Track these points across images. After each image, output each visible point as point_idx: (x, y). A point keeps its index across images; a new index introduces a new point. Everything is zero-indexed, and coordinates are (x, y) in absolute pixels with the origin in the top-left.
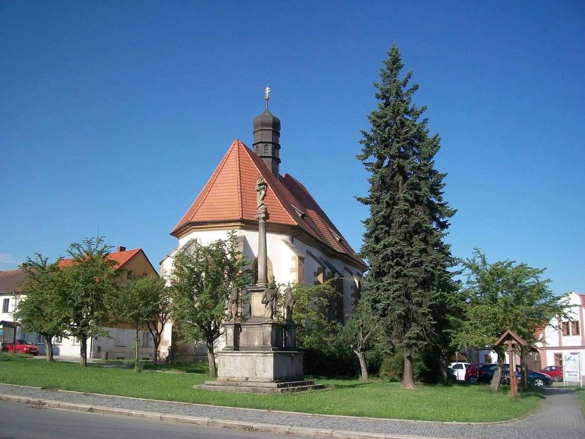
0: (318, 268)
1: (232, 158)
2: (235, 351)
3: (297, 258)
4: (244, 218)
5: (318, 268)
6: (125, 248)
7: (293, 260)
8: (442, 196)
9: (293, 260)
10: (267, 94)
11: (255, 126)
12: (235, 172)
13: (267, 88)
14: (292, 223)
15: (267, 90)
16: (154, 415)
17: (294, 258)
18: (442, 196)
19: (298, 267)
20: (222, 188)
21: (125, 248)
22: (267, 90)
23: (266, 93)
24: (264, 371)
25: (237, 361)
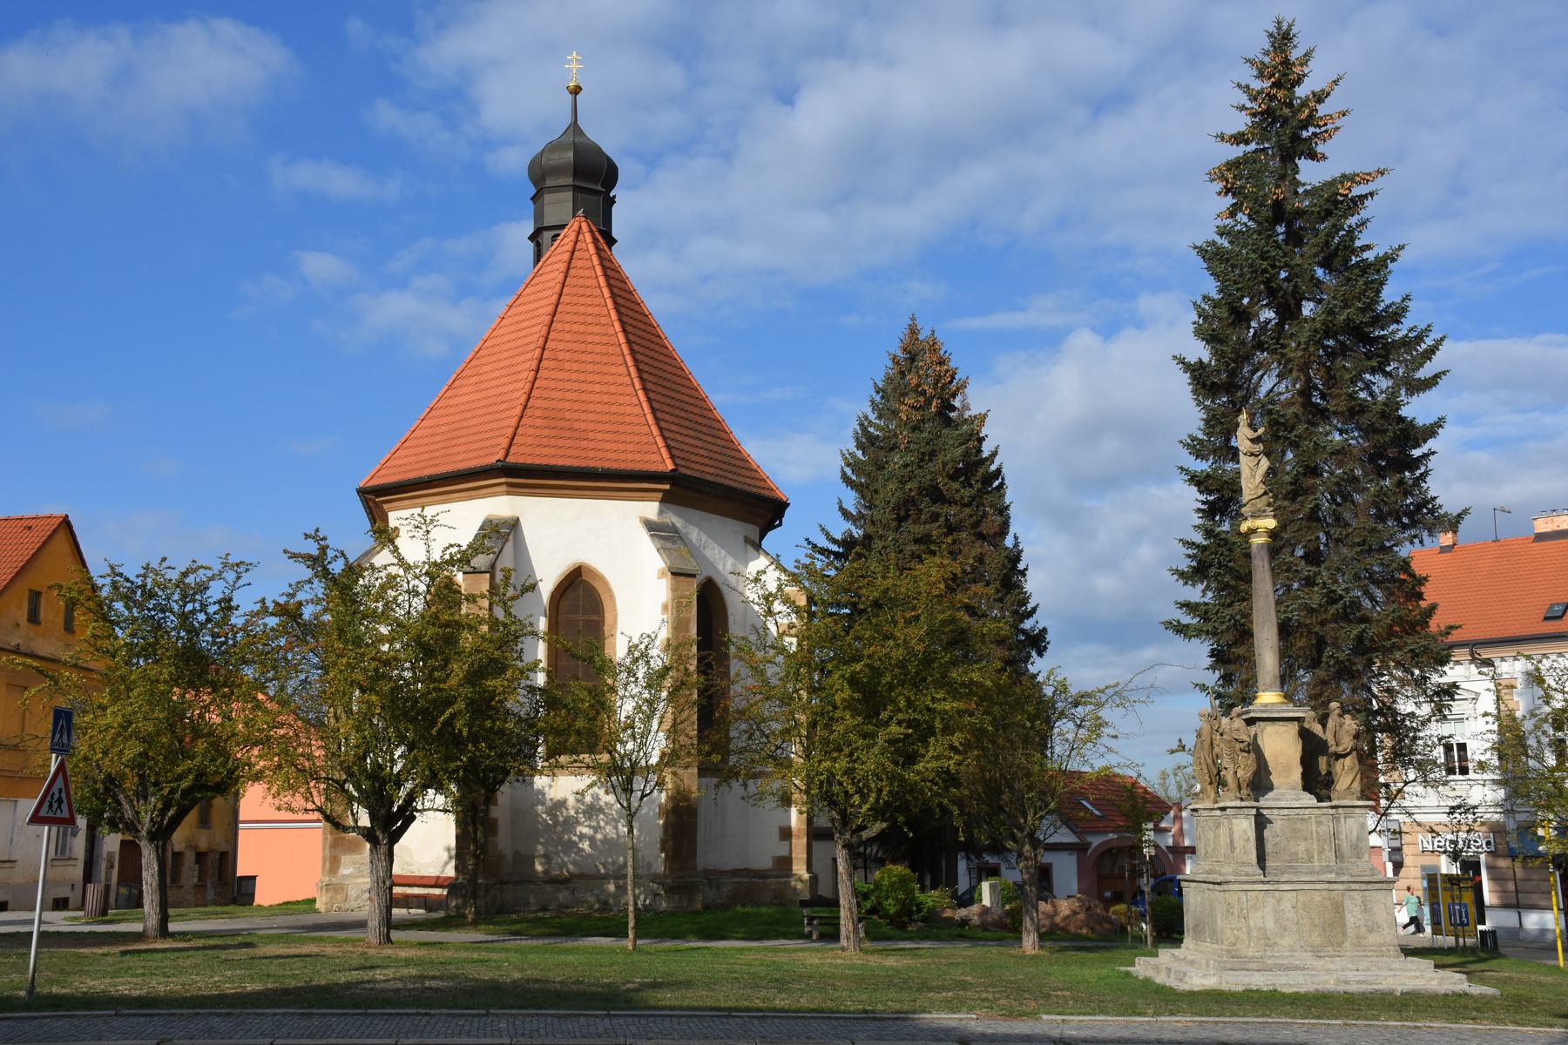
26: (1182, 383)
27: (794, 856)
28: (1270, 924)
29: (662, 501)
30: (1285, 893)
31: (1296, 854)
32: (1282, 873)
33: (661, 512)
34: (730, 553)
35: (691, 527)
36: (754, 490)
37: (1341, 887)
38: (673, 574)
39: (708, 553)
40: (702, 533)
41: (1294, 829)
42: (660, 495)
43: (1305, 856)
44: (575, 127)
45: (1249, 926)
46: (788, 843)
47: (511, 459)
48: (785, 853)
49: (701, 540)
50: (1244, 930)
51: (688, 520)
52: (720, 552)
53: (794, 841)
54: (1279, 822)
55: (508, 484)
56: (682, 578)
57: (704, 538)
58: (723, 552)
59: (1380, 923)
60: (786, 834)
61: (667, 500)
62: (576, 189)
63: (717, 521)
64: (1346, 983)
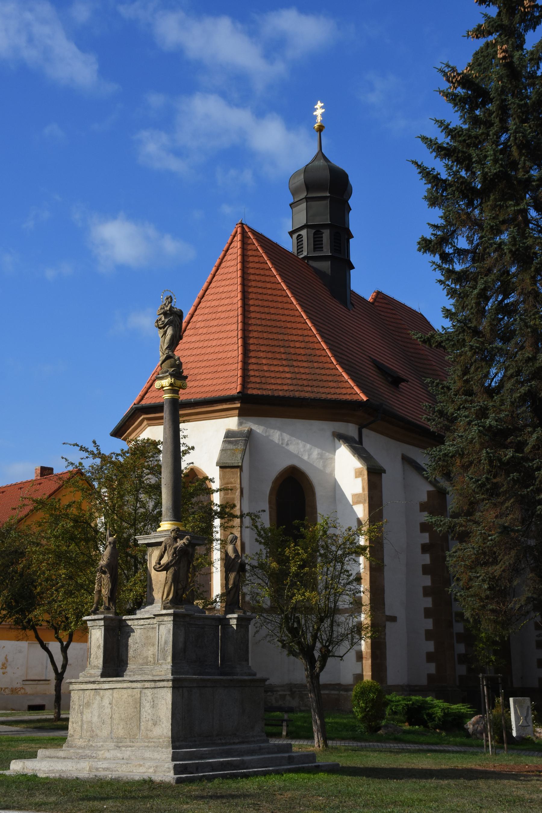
0: (429, 493)
1: (229, 264)
2: (105, 679)
3: (366, 472)
4: (250, 392)
5: (429, 493)
6: (52, 469)
7: (356, 477)
8: (431, 150)
9: (356, 477)
10: (319, 119)
11: (294, 192)
12: (232, 294)
13: (319, 104)
14: (355, 398)
15: (319, 111)
16: (210, 761)
17: (358, 474)
18: (431, 150)
19: (366, 492)
20: (205, 331)
21: (52, 469)
22: (319, 111)
23: (316, 116)
24: (155, 724)
25: (106, 702)
26: (425, 254)
27: (364, 673)
28: (95, 719)
29: (240, 415)
30: (106, 691)
31: (147, 657)
32: (134, 675)
33: (240, 424)
34: (315, 445)
35: (272, 431)
36: (329, 397)
37: (139, 685)
38: (221, 467)
39: (292, 448)
40: (284, 434)
41: (147, 637)
42: (237, 412)
43: (152, 660)
44: (321, 155)
45: (82, 720)
46: (360, 663)
47: (143, 402)
48: (358, 672)
49: (283, 440)
50: (80, 723)
51: (259, 424)
52: (304, 446)
53: (364, 662)
54: (139, 631)
55: (149, 419)
56: (228, 470)
57: (286, 437)
58: (308, 446)
59: (161, 717)
60: (360, 656)
61: (243, 414)
62: (307, 199)
63: (300, 424)
64: (97, 769)
